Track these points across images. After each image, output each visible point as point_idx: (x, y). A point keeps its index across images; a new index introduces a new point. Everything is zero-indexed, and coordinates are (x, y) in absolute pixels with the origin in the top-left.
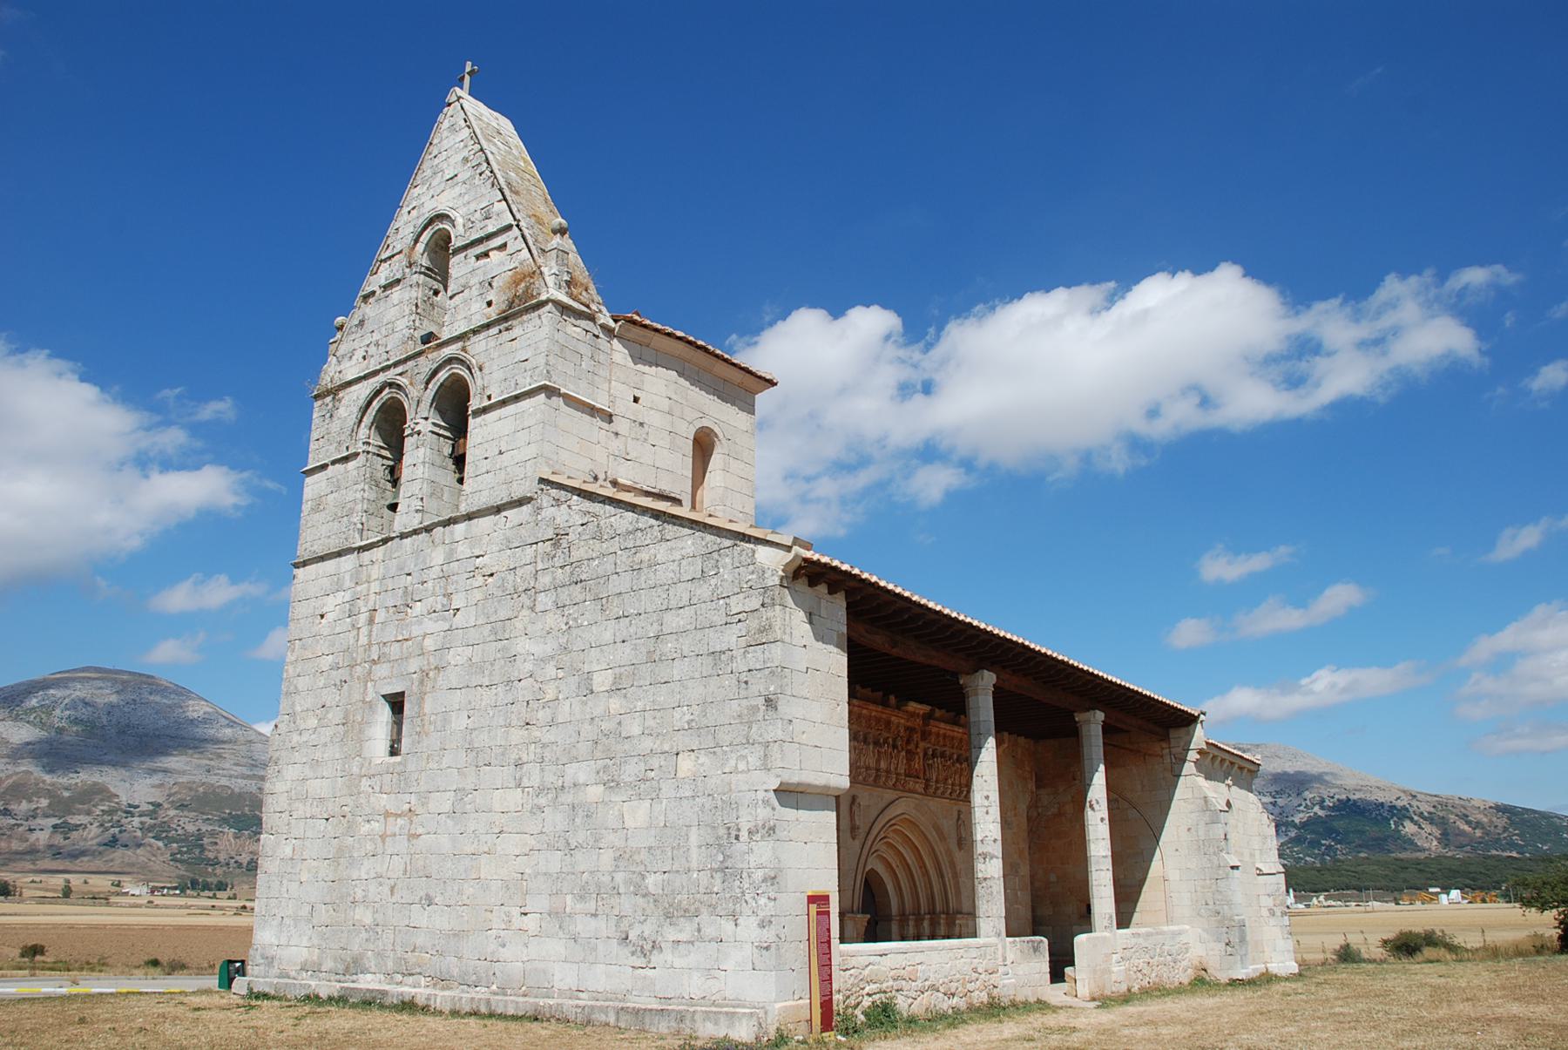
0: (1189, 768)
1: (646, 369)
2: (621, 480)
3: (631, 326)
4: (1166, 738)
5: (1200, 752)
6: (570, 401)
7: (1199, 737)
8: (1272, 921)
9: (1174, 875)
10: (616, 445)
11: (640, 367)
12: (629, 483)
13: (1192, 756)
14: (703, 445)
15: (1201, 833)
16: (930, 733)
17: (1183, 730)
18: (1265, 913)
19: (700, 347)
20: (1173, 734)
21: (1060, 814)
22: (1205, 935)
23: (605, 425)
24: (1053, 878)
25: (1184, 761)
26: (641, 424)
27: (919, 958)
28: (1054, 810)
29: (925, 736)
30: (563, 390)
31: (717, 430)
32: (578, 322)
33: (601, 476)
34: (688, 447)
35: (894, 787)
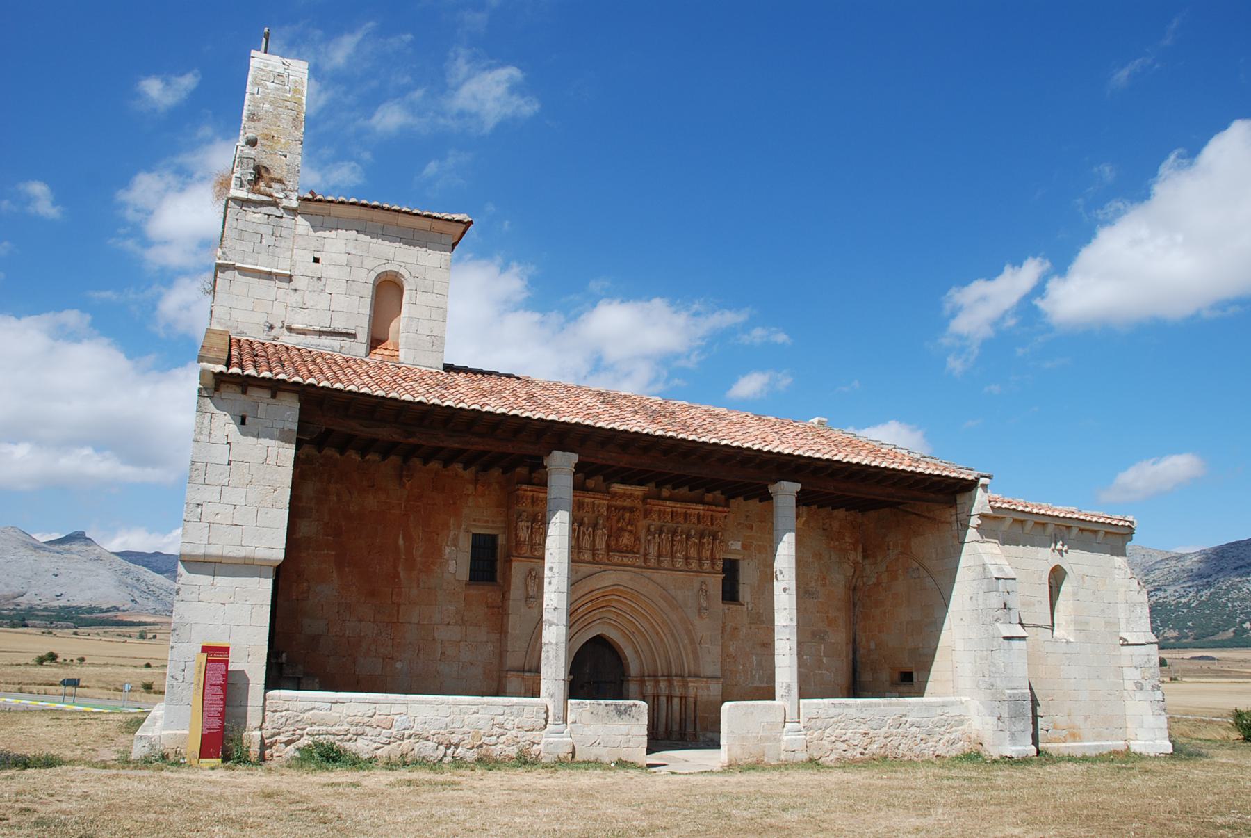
0: (972, 534)
1: (327, 233)
2: (294, 326)
3: (308, 203)
4: (953, 504)
5: (982, 516)
6: (244, 272)
7: (981, 501)
8: (1139, 695)
9: (960, 646)
10: (294, 299)
11: (320, 233)
12: (300, 327)
13: (975, 521)
14: (388, 291)
15: (980, 602)
16: (651, 511)
17: (967, 495)
18: (1130, 686)
19: (375, 207)
20: (960, 499)
21: (878, 584)
22: (981, 708)
23: (285, 285)
24: (873, 646)
25: (968, 527)
26: (319, 279)
27: (396, 709)
28: (874, 580)
29: (647, 514)
30: (238, 265)
31: (402, 271)
32: (259, 210)
33: (278, 325)
34: (368, 291)
35: (594, 562)
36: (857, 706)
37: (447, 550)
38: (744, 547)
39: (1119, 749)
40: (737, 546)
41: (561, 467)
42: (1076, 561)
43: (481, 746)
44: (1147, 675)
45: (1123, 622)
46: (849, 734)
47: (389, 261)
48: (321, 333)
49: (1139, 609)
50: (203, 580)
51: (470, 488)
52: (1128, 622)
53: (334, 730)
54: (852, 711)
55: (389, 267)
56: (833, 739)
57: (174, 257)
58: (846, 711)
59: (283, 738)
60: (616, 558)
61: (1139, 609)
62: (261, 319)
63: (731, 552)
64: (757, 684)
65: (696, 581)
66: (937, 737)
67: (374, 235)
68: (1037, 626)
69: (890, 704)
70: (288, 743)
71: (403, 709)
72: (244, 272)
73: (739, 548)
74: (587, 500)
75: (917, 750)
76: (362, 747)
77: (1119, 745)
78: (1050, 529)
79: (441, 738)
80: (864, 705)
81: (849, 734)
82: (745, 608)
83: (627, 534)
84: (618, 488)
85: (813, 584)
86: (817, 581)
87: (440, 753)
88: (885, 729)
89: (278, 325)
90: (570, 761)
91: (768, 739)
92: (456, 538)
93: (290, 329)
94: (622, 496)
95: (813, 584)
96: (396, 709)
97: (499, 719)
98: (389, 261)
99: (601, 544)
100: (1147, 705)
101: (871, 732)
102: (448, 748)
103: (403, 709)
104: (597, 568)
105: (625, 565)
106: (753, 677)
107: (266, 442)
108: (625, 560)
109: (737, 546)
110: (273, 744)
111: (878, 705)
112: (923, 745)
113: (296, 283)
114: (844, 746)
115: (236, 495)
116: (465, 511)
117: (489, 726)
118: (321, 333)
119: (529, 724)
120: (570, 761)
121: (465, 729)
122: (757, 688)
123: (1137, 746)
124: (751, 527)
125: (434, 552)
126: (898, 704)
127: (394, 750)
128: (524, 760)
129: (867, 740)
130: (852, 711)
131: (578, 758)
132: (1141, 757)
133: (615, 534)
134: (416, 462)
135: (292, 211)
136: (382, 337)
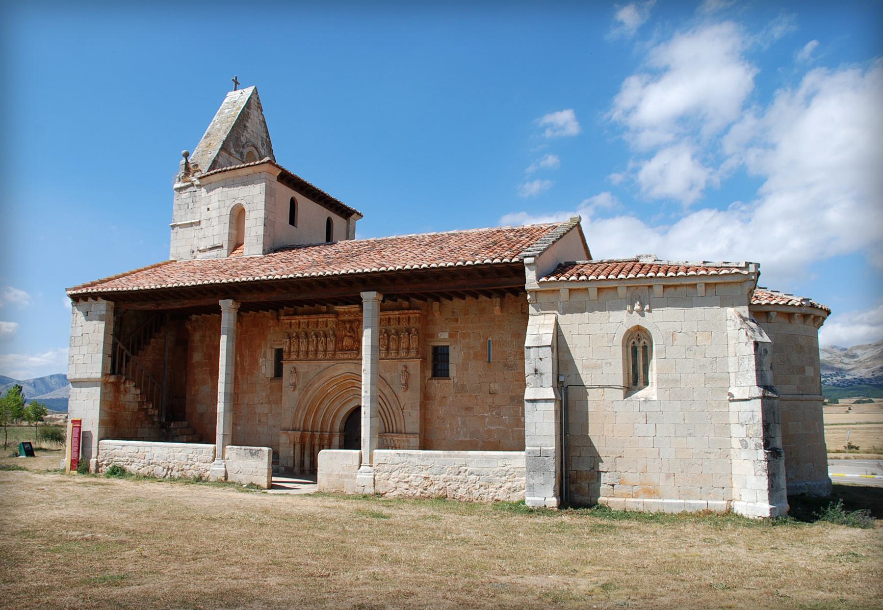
6: (181, 226)
8: (744, 454)
18: (735, 443)
23: (198, 227)
33: (196, 250)
36: (419, 456)
37: (261, 360)
38: (451, 336)
39: (667, 511)
40: (445, 335)
41: (228, 307)
42: (661, 321)
43: (182, 470)
44: (751, 432)
45: (732, 375)
46: (411, 477)
47: (236, 199)
48: (211, 249)
49: (746, 361)
50: (77, 390)
51: (271, 323)
52: (736, 377)
53: (122, 459)
54: (414, 460)
55: (237, 202)
56: (397, 480)
57: (646, 140)
58: (409, 459)
59: (105, 463)
60: (339, 355)
61: (746, 361)
62: (188, 249)
63: (440, 341)
64: (461, 438)
65: (400, 366)
66: (498, 485)
67: (229, 186)
68: (604, 387)
69: (450, 456)
70: (107, 465)
71: (149, 449)
72: (181, 226)
73: (447, 337)
74: (320, 320)
75: (476, 494)
76: (132, 468)
77: (718, 504)
78: (622, 291)
79: (164, 465)
80: (425, 455)
81: (411, 477)
82: (451, 382)
83: (346, 338)
84: (340, 308)
85: (512, 358)
86: (515, 356)
87: (165, 473)
88: (444, 475)
89: (196, 250)
90: (225, 481)
91: (346, 476)
92: (265, 352)
93: (200, 251)
94: (345, 313)
95: (512, 358)
96: (147, 449)
97: (191, 456)
98: (236, 199)
99: (331, 347)
100: (749, 465)
101: (432, 476)
102: (168, 470)
103: (149, 449)
104: (332, 362)
105: (351, 359)
106: (458, 433)
107: (94, 322)
108: (346, 356)
109: (445, 335)
110: (102, 466)
111: (439, 456)
112: (482, 490)
113: (203, 224)
114: (406, 486)
115: (84, 350)
116: (269, 336)
117: (184, 461)
118: (211, 249)
119: (204, 459)
120: (225, 481)
121: (176, 461)
122: (462, 441)
123: (739, 508)
124: (457, 320)
125: (255, 362)
126: (458, 456)
127: (144, 471)
128: (199, 479)
129: (427, 483)
130: (414, 460)
131: (229, 480)
132: (740, 517)
133: (338, 340)
134: (446, 302)
135: (199, 186)
136: (240, 243)
